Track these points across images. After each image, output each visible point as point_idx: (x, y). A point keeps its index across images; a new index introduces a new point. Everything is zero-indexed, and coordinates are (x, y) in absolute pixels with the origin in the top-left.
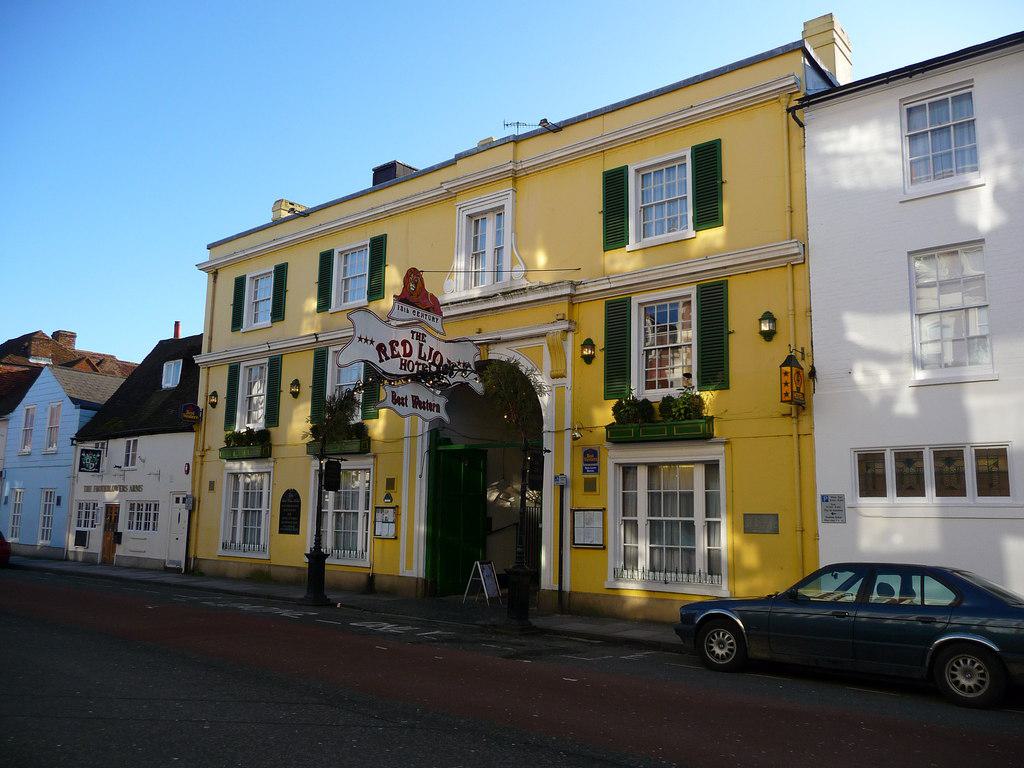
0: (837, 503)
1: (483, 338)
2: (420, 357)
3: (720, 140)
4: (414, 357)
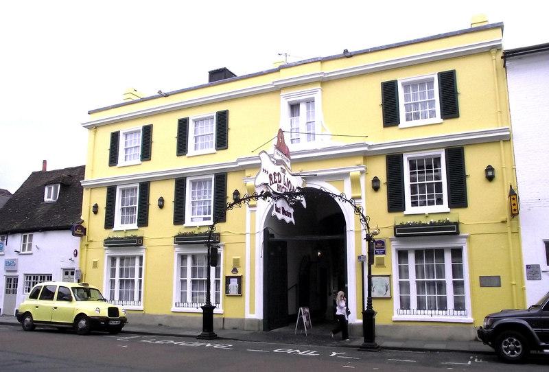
3: (455, 70)
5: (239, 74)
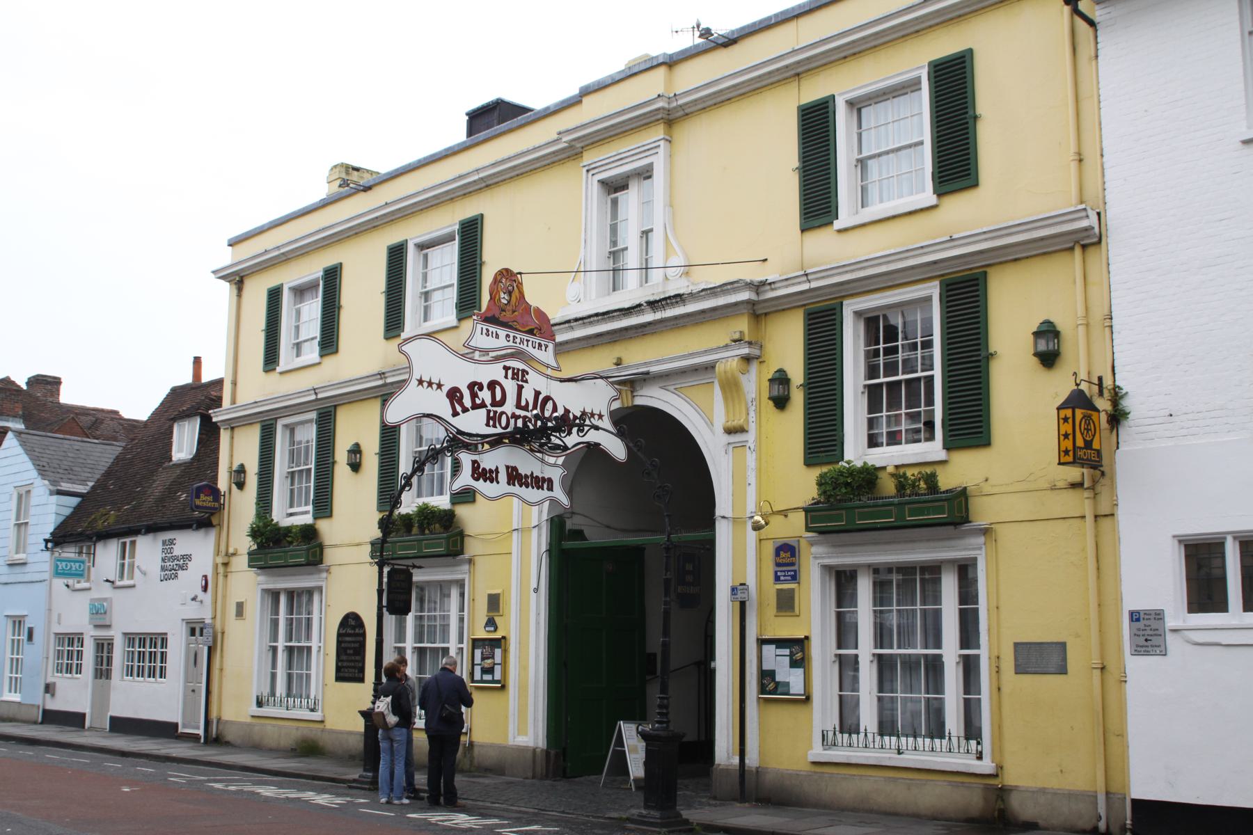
0: (1154, 624)
1: (625, 373)
2: (518, 406)
3: (482, 215)
4: (509, 407)
5: (537, 103)
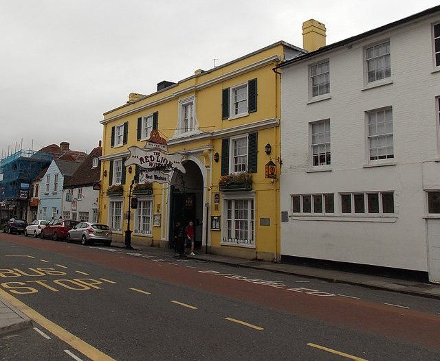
2: (157, 161)
